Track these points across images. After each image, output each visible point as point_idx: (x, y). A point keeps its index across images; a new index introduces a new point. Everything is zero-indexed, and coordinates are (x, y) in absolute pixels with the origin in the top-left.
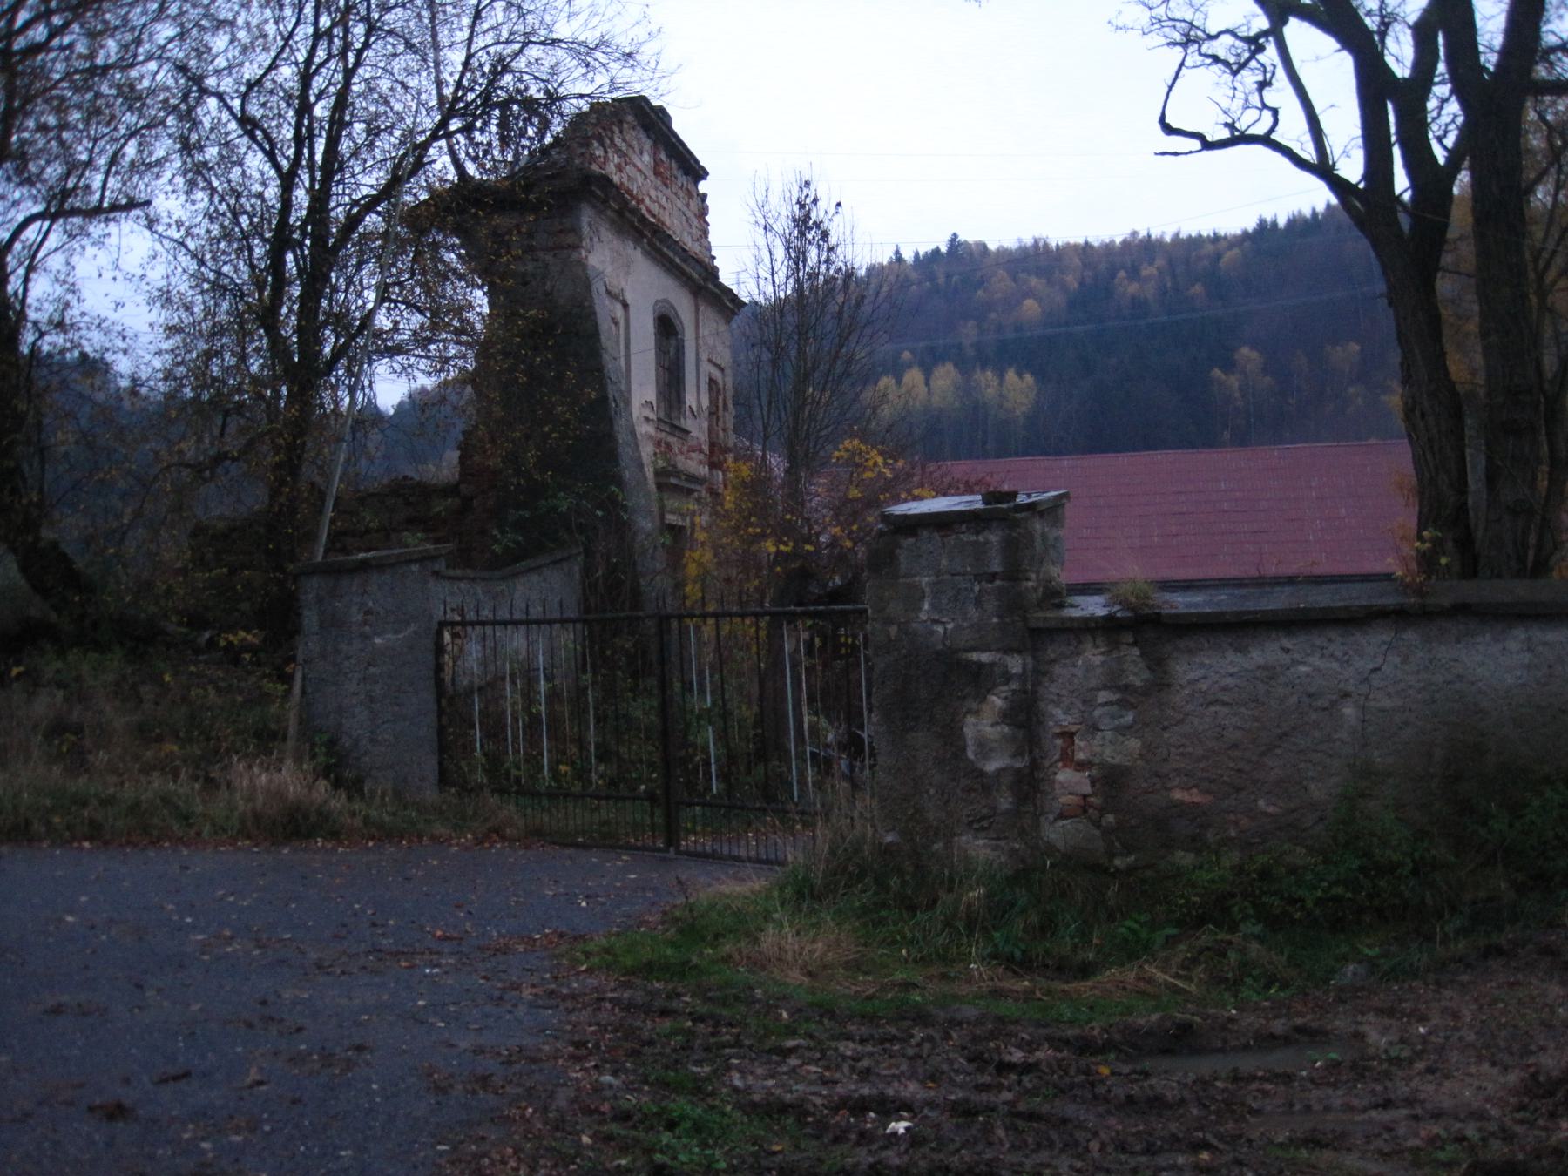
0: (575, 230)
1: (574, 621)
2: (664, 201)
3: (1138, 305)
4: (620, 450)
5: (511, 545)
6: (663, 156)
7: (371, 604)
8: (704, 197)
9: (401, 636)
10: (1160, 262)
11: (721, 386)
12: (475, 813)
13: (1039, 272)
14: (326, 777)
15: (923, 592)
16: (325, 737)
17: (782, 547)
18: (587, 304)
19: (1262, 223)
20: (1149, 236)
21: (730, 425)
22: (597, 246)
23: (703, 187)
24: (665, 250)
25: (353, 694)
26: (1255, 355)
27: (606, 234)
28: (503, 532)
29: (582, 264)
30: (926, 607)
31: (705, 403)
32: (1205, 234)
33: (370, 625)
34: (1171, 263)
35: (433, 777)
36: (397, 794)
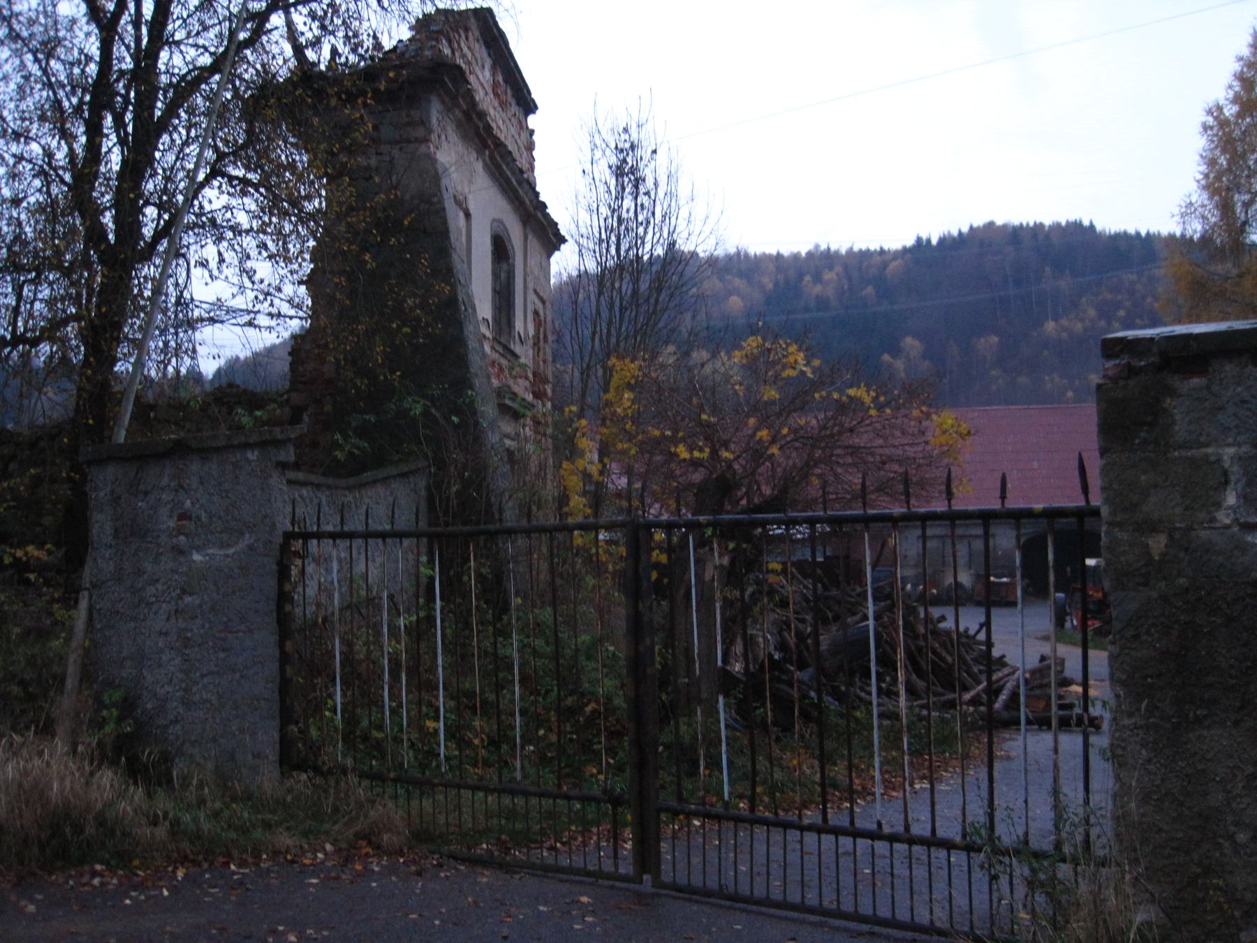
0: (424, 122)
2: (500, 123)
3: (822, 303)
5: (356, 451)
6: (500, 79)
7: (188, 503)
8: (532, 132)
9: (231, 551)
10: (838, 269)
11: (542, 318)
12: (336, 810)
13: (741, 274)
14: (114, 763)
15: (1225, 473)
16: (117, 695)
17: (696, 454)
18: (435, 199)
19: (919, 239)
20: (829, 249)
22: (445, 144)
23: (532, 121)
24: (504, 167)
25: (160, 633)
26: (917, 343)
27: (453, 136)
28: (346, 437)
29: (433, 161)
30: (1231, 499)
31: (531, 332)
32: (872, 248)
33: (186, 535)
34: (846, 267)
35: (272, 754)
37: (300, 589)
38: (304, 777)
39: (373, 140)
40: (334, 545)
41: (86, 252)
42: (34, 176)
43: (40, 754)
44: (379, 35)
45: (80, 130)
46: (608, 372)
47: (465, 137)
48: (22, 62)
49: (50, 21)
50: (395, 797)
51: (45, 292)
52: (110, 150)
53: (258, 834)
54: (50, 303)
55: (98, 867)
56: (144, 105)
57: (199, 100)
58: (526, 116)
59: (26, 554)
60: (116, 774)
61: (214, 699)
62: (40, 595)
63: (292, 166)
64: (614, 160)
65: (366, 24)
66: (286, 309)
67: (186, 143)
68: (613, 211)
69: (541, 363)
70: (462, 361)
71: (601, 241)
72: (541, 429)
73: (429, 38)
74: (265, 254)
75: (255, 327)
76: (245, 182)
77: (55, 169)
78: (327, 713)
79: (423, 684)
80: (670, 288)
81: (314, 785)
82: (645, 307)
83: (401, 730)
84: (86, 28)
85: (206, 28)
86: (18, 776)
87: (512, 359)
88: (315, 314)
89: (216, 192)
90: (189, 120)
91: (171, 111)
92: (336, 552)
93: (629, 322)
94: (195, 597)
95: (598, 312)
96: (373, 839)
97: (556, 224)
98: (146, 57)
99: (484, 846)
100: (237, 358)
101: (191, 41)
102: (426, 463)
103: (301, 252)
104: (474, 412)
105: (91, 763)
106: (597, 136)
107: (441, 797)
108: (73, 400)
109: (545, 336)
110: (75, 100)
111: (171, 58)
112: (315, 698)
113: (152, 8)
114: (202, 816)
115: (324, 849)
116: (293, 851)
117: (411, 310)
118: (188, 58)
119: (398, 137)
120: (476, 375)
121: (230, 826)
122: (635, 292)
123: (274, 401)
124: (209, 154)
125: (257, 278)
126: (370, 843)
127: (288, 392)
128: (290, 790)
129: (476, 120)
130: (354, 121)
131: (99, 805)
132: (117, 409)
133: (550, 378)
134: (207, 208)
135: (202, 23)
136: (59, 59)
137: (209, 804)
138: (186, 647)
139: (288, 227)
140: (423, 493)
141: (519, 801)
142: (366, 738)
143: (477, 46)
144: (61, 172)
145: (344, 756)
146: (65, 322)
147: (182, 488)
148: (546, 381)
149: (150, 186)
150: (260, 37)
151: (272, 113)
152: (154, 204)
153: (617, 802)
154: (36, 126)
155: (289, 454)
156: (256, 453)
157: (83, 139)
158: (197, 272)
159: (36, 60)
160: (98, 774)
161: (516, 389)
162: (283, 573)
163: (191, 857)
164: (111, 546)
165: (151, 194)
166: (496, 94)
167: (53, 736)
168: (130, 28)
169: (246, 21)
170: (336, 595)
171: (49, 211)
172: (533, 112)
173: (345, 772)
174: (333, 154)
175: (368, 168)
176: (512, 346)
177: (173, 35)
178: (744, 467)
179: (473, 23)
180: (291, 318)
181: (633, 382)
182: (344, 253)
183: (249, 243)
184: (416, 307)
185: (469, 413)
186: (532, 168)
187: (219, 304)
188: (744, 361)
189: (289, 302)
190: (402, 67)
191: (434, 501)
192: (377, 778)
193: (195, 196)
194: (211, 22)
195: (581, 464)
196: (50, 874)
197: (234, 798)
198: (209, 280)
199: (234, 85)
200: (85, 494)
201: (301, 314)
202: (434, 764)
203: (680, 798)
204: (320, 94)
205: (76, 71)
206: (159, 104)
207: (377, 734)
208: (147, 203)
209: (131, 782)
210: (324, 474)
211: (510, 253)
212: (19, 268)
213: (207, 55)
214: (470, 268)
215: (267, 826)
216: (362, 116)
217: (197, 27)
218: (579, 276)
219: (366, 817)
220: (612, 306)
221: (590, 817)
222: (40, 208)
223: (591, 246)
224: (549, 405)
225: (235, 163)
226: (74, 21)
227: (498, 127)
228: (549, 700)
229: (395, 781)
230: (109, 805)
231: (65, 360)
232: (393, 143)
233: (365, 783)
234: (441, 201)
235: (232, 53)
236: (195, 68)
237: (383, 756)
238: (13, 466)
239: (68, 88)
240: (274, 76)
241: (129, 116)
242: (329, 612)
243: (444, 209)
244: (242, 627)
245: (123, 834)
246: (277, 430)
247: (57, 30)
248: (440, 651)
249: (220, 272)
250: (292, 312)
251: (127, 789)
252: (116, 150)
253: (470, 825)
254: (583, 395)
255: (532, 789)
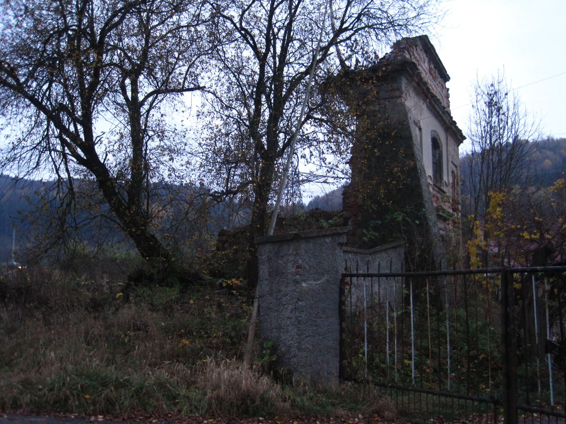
0: (399, 89)
1: (398, 275)
2: (433, 86)
4: (424, 193)
5: (373, 237)
6: (432, 66)
7: (300, 261)
8: (448, 90)
9: (319, 282)
11: (456, 174)
12: (364, 399)
13: (550, 149)
14: (269, 373)
16: (270, 344)
17: (533, 236)
18: (405, 123)
21: (460, 192)
22: (409, 98)
23: (448, 85)
25: (288, 318)
27: (412, 94)
28: (368, 231)
29: (403, 105)
31: (451, 181)
33: (299, 275)
35: (336, 372)
36: (314, 383)
37: (349, 299)
38: (350, 383)
39: (376, 98)
40: (364, 280)
41: (256, 155)
42: (234, 124)
43: (238, 368)
44: (377, 52)
45: (252, 103)
46: (489, 198)
47: (417, 94)
48: (229, 77)
49: (240, 60)
50: (391, 395)
51: (239, 172)
52: (264, 111)
53: (329, 408)
54: (241, 176)
55: (261, 418)
56: (278, 90)
57: (301, 86)
58: (445, 82)
59: (232, 282)
60: (269, 378)
61: (311, 347)
62: (237, 300)
63: (341, 112)
64: (487, 100)
65: (371, 48)
66: (340, 175)
67: (296, 105)
68: (488, 123)
69: (456, 195)
70: (420, 195)
71: (482, 137)
72: (456, 225)
73: (400, 51)
74: (330, 151)
75: (327, 183)
76: (321, 120)
77: (242, 120)
78: (360, 355)
79: (405, 344)
80: (516, 157)
81: (354, 387)
82: (504, 168)
83: (394, 364)
84: (253, 61)
85: (303, 56)
86: (229, 378)
87: (442, 194)
88: (353, 177)
89: (309, 125)
90: (297, 96)
91: (289, 92)
92: (366, 282)
93: (497, 174)
94: (303, 302)
95: (482, 170)
96: (381, 414)
97: (461, 131)
98: (278, 71)
99: (432, 420)
100: (318, 197)
101: (296, 62)
102: (404, 242)
103: (347, 149)
104: (426, 218)
105: (259, 373)
106: (478, 89)
107: (411, 396)
108: (251, 217)
109: (457, 183)
110: (250, 91)
111: (288, 70)
112: (355, 348)
113: (280, 49)
114: (305, 398)
115: (358, 417)
116: (345, 417)
117: (396, 173)
118: (296, 69)
119: (387, 96)
120: (427, 202)
121: (317, 404)
122: (500, 161)
123: (336, 215)
124: (306, 109)
125: (327, 162)
126: (379, 416)
127: (342, 211)
128: (343, 389)
129: (423, 86)
130: (368, 91)
131: (262, 392)
132: (269, 220)
133: (460, 202)
134: (306, 132)
135: (301, 54)
136: (243, 74)
137: (308, 394)
138: (299, 324)
139: (340, 139)
140: (403, 256)
141: (449, 400)
142: (377, 367)
143: (421, 53)
144: (245, 121)
145: (368, 375)
146: (248, 184)
147: (298, 254)
148: (458, 204)
149: (281, 125)
150: (326, 57)
151: (332, 90)
152: (283, 132)
153: (496, 403)
154: (234, 103)
155: (344, 239)
156: (330, 239)
157: (254, 107)
158: (302, 161)
159: (235, 76)
160: (261, 378)
161: (444, 207)
162: (342, 292)
163: (300, 417)
164: (267, 280)
165: (282, 128)
166: (431, 74)
167: (243, 361)
168: (271, 59)
169: (320, 51)
170: (365, 302)
171: (241, 137)
172: (448, 81)
173: (368, 382)
174: (359, 105)
175: (374, 111)
176: (442, 188)
177: (289, 60)
178: (557, 242)
179: (419, 43)
180: (343, 178)
181: (501, 202)
182: (366, 149)
183: (323, 146)
184: (398, 172)
185: (424, 219)
186: (449, 106)
187: (311, 173)
188: (556, 191)
189: (342, 172)
190: (388, 65)
191: (408, 259)
192: (382, 385)
193: (301, 128)
194: (305, 53)
195: (477, 241)
196: (241, 420)
197: (319, 392)
198: (306, 164)
199: (315, 79)
200: (257, 257)
201: (347, 177)
202: (408, 380)
203: (528, 403)
204: (353, 80)
205: (250, 79)
206: (284, 90)
207: (383, 366)
208: (280, 132)
209: (275, 382)
210: (358, 248)
211: (440, 145)
212: (229, 162)
213: (303, 67)
214: (422, 152)
215: (333, 405)
216: (371, 88)
217: (299, 56)
218: (473, 154)
219: (377, 403)
220: (488, 167)
221: (482, 409)
222: (236, 137)
223: (478, 140)
224: (460, 214)
225: (316, 112)
226: (249, 59)
227: (433, 88)
228: (462, 352)
229: (391, 387)
230: (265, 392)
231: (247, 199)
232: (385, 99)
233: (377, 388)
234: (408, 124)
235: (314, 65)
236: (299, 73)
237: (385, 375)
238: (226, 245)
239: (247, 86)
240: (332, 74)
241: (272, 96)
242: (362, 308)
243: (409, 127)
244: (323, 316)
245: (271, 405)
246: (339, 228)
247: (242, 63)
248: (412, 329)
249: (311, 160)
250: (343, 176)
251: (273, 386)
252: (267, 110)
253: (425, 410)
254: (476, 208)
255: (456, 394)
